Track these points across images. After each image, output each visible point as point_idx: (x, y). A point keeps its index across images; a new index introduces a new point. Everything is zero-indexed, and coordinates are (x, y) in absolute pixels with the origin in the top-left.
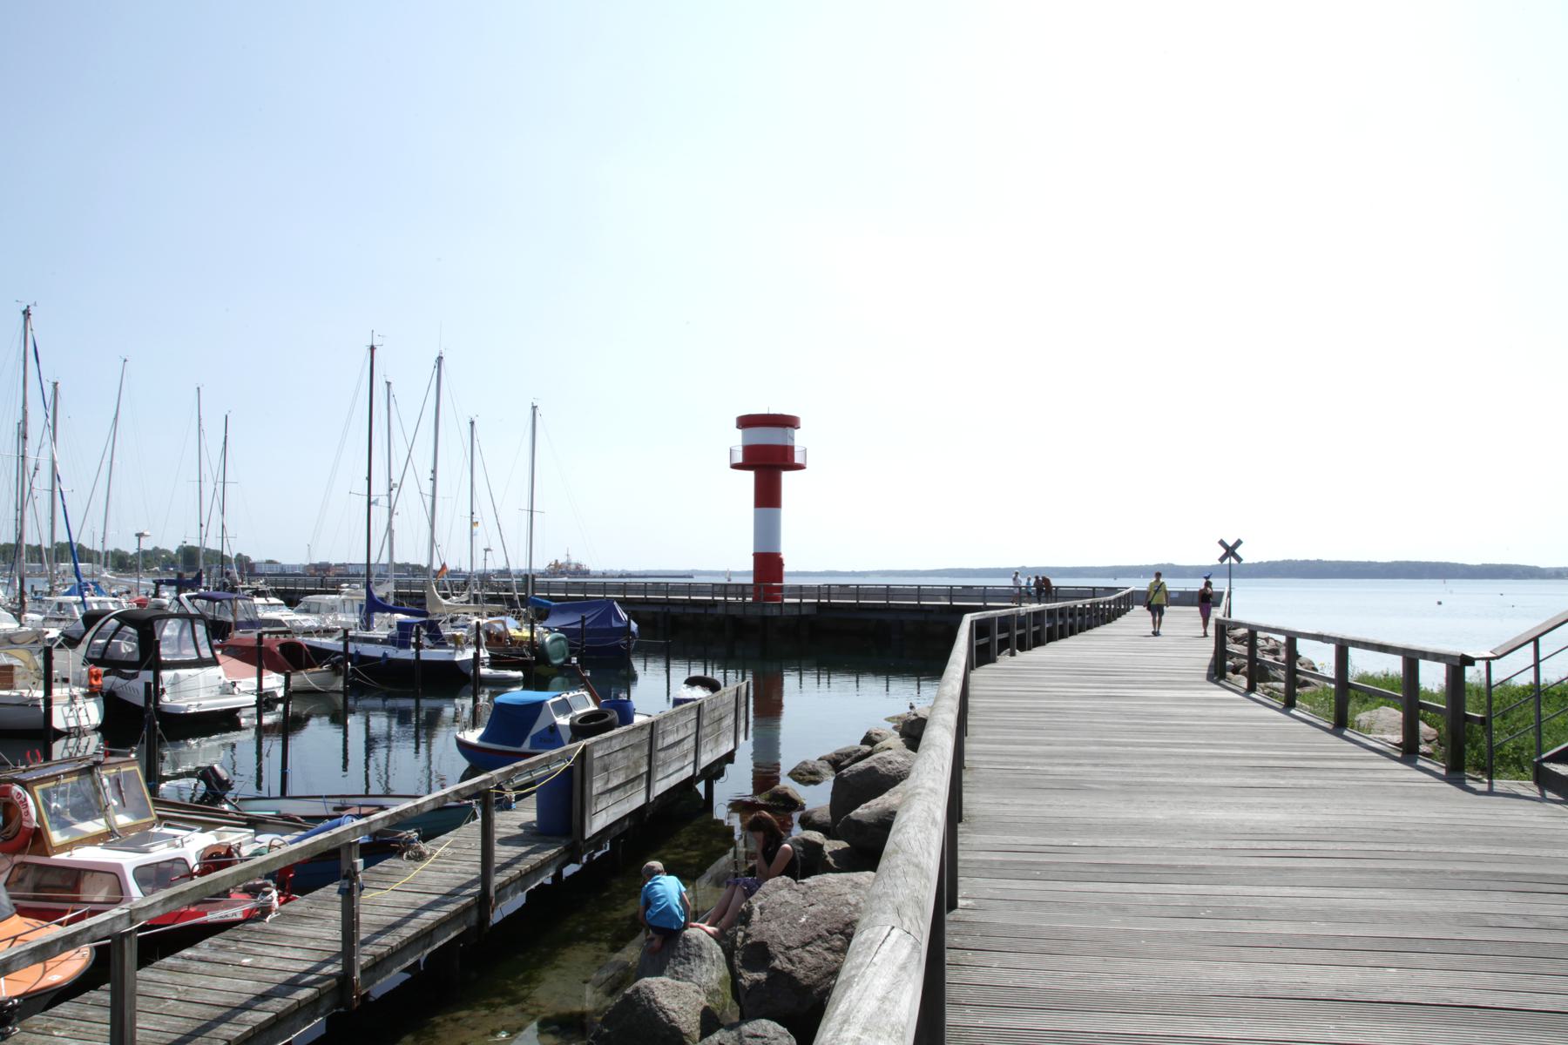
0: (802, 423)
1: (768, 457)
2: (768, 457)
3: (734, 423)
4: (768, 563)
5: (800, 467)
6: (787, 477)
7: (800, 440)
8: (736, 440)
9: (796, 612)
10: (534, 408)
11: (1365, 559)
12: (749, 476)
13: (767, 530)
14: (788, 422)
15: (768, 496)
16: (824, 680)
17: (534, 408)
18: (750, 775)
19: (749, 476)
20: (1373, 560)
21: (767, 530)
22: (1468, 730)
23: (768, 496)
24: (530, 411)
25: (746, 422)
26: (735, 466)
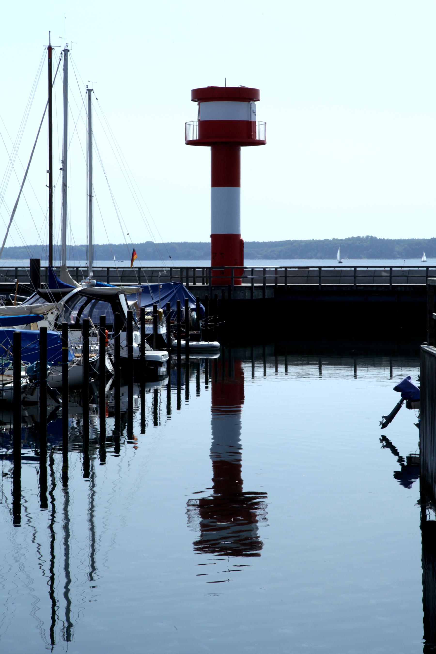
0: (262, 96)
1: (226, 129)
2: (226, 129)
3: (189, 96)
4: (227, 245)
5: (261, 143)
6: (246, 153)
7: (263, 113)
8: (191, 113)
9: (248, 296)
10: (90, 91)
11: (198, 241)
12: (206, 152)
13: (225, 208)
14: (247, 95)
15: (226, 174)
16: (282, 369)
17: (90, 91)
18: (210, 463)
19: (206, 152)
20: (281, 240)
21: (225, 208)
22: (61, 627)
23: (226, 174)
24: (85, 96)
25: (202, 95)
26: (190, 143)
